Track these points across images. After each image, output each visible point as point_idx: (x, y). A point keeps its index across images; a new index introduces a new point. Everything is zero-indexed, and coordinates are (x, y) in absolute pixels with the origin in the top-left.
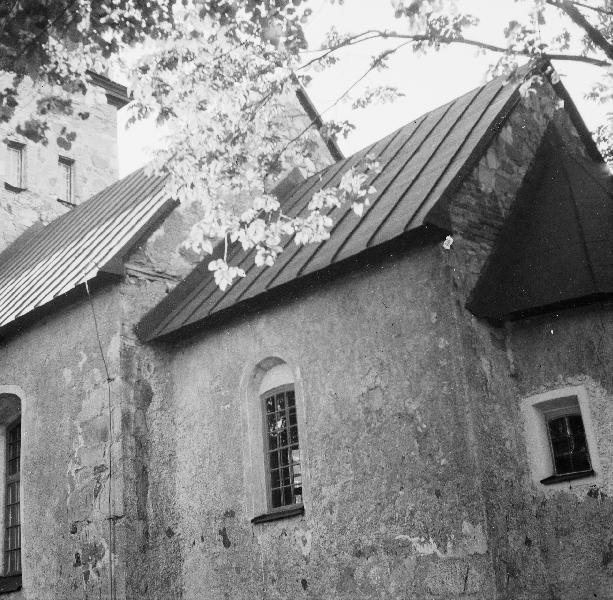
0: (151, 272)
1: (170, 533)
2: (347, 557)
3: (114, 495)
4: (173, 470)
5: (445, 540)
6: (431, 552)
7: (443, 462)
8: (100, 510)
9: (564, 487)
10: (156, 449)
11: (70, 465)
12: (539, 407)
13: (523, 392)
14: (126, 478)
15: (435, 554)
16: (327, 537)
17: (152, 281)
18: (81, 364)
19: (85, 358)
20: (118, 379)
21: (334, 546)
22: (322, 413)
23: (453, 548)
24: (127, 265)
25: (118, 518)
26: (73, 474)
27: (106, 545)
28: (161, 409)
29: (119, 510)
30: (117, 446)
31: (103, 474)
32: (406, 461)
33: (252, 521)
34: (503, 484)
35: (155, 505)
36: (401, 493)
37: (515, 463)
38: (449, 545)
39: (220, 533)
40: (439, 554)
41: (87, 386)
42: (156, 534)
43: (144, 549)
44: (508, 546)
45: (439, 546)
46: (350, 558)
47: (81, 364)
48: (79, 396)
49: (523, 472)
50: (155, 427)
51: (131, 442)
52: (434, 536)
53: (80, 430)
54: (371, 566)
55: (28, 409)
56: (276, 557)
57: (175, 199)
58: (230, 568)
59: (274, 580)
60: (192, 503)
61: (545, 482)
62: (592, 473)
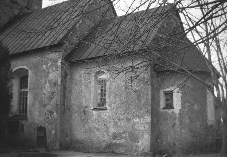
0: (69, 43)
1: (69, 110)
2: (116, 120)
3: (57, 99)
4: (71, 95)
5: (141, 119)
6: (137, 121)
7: (143, 102)
8: (53, 102)
9: (167, 110)
10: (68, 89)
11: (44, 90)
12: (164, 92)
13: (161, 88)
14: (61, 96)
15: (138, 122)
16: (112, 115)
17: (69, 45)
18: (49, 65)
19: (50, 63)
20: (60, 71)
21: (113, 117)
22: (114, 87)
23: (142, 121)
24: (64, 41)
25: (58, 105)
26: (45, 93)
27: (54, 111)
28: (69, 79)
29: (59, 103)
30: (59, 87)
31: (54, 94)
32: (134, 101)
33: (93, 109)
34: (155, 108)
35: (67, 103)
36: (132, 108)
37: (158, 104)
38: (142, 120)
39: (83, 111)
40: (139, 121)
41: (50, 71)
42: (66, 109)
43: (64, 113)
44: (154, 121)
45: (139, 120)
46: (117, 120)
47: (49, 65)
48: (48, 73)
49: (159, 106)
50: (68, 84)
51: (62, 87)
52: (138, 118)
53: (48, 82)
54: (122, 123)
55: (31, 74)
56: (98, 118)
57: (93, 110)
58: (85, 120)
59: (97, 123)
60: (75, 103)
61: (163, 108)
62: (173, 108)
